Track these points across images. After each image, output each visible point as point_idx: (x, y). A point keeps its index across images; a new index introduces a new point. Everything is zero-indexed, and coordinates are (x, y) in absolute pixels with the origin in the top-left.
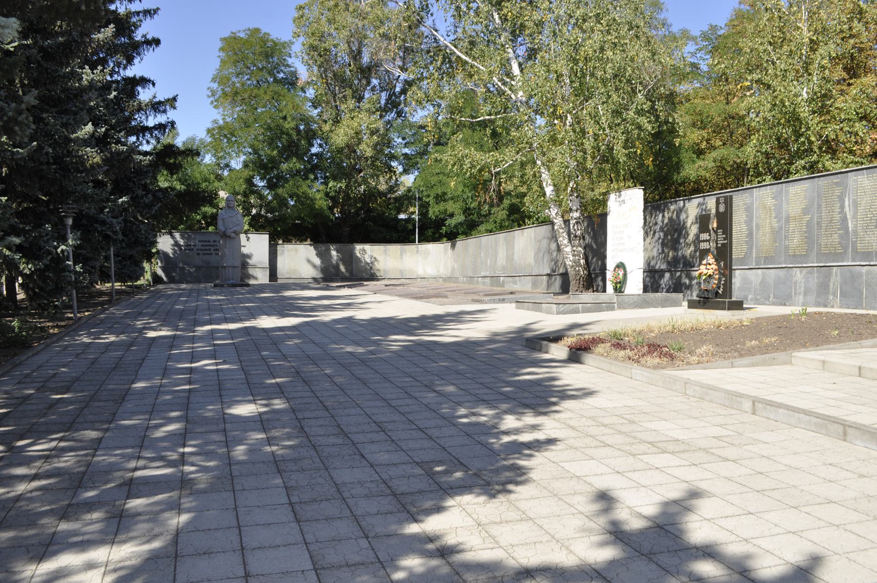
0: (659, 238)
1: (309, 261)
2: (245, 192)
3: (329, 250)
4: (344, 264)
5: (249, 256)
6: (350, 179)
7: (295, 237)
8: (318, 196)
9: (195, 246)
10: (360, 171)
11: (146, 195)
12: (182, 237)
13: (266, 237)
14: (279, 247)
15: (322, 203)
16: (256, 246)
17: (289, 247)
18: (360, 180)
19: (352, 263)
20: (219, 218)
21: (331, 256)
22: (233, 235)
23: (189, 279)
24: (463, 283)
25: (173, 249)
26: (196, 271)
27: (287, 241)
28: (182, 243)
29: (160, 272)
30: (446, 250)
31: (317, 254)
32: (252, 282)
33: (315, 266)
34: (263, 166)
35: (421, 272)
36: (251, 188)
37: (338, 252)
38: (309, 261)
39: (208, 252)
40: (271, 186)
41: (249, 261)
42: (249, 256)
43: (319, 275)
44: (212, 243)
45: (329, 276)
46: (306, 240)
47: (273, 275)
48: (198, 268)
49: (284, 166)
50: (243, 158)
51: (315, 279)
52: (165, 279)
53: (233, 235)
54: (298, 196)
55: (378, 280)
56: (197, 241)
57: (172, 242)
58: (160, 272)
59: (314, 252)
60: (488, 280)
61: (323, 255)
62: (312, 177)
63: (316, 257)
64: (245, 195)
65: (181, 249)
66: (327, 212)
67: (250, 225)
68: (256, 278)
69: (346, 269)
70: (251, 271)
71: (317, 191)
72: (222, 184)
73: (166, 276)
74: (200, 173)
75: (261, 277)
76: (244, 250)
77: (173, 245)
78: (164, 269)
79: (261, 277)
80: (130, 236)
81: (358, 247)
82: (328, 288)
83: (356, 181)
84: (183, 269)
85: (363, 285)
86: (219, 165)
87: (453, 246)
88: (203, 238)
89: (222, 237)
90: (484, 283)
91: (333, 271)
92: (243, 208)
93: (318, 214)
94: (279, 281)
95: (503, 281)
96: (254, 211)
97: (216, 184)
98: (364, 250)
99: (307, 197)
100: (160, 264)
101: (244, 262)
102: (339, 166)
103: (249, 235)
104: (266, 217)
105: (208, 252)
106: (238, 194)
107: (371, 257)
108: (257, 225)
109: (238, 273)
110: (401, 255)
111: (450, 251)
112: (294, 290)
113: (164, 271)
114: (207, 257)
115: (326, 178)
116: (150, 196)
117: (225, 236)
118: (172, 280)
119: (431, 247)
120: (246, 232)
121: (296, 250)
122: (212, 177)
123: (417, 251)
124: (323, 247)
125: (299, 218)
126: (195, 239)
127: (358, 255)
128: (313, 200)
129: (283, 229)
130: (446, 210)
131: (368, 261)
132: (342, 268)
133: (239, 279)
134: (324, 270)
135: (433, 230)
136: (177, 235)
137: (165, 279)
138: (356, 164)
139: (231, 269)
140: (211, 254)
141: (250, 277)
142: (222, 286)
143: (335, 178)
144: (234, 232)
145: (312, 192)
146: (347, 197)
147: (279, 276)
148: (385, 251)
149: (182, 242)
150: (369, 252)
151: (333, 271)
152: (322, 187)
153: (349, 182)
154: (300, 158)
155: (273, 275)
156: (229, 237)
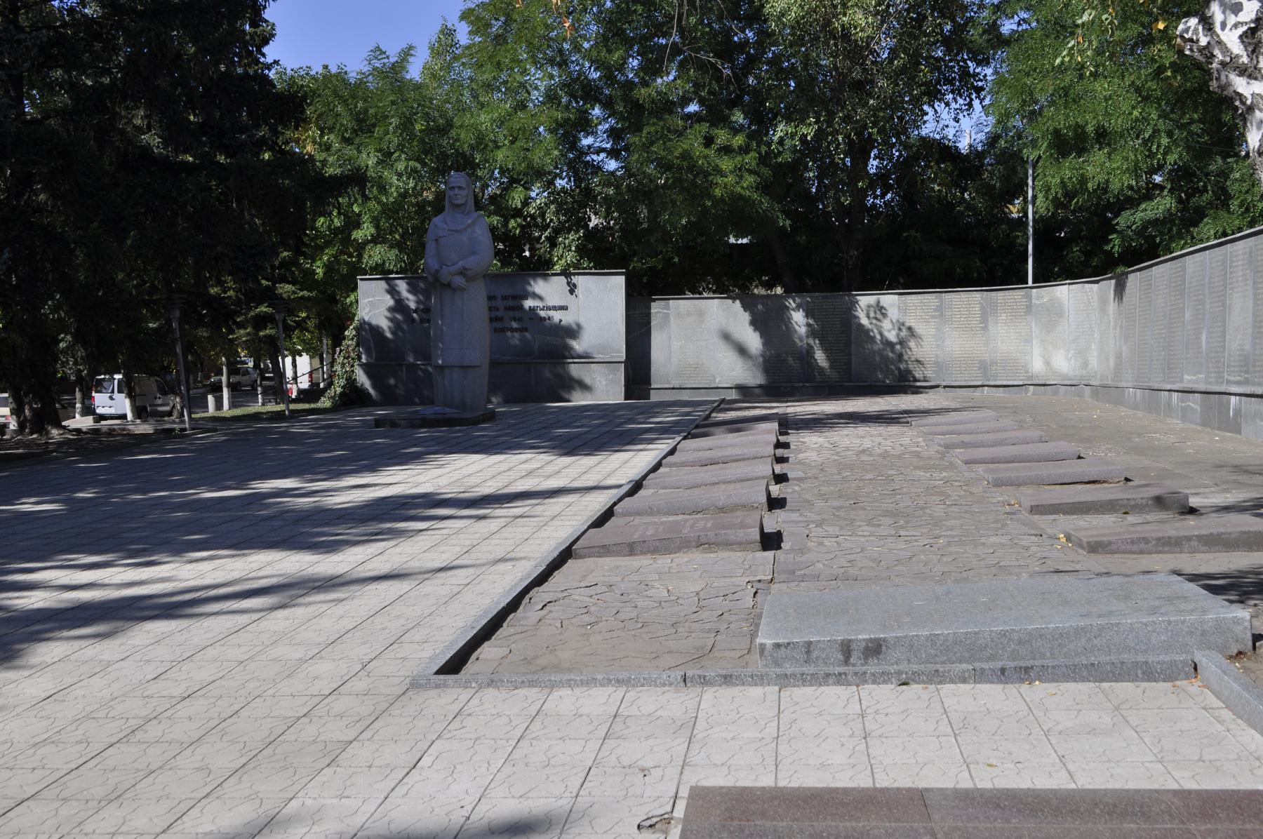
0: (295, 378)
1: (726, 337)
4: (826, 350)
5: (572, 332)
6: (831, 115)
12: (413, 289)
13: (617, 284)
14: (656, 308)
16: (590, 307)
21: (789, 329)
22: (459, 281)
24: (1135, 407)
28: (413, 306)
29: (362, 378)
30: (1103, 302)
32: (579, 400)
33: (742, 350)
35: (1037, 366)
38: (726, 337)
42: (572, 332)
51: (743, 390)
55: (917, 391)
57: (390, 302)
58: (362, 378)
59: (746, 317)
60: (1194, 402)
61: (768, 321)
67: (581, 250)
69: (829, 358)
73: (374, 386)
77: (391, 309)
78: (368, 369)
79: (604, 388)
81: (865, 301)
87: (1120, 290)
90: (1185, 414)
94: (655, 397)
95: (1238, 412)
98: (880, 308)
103: (575, 279)
107: (900, 326)
108: (599, 255)
110: (984, 320)
111: (1112, 306)
113: (369, 374)
118: (388, 397)
119: (1064, 293)
121: (701, 314)
123: (1029, 308)
127: (864, 321)
130: (1083, 180)
131: (892, 336)
132: (820, 357)
135: (1087, 245)
136: (402, 286)
148: (939, 309)
150: (893, 313)
153: (830, 122)
156: (449, 285)
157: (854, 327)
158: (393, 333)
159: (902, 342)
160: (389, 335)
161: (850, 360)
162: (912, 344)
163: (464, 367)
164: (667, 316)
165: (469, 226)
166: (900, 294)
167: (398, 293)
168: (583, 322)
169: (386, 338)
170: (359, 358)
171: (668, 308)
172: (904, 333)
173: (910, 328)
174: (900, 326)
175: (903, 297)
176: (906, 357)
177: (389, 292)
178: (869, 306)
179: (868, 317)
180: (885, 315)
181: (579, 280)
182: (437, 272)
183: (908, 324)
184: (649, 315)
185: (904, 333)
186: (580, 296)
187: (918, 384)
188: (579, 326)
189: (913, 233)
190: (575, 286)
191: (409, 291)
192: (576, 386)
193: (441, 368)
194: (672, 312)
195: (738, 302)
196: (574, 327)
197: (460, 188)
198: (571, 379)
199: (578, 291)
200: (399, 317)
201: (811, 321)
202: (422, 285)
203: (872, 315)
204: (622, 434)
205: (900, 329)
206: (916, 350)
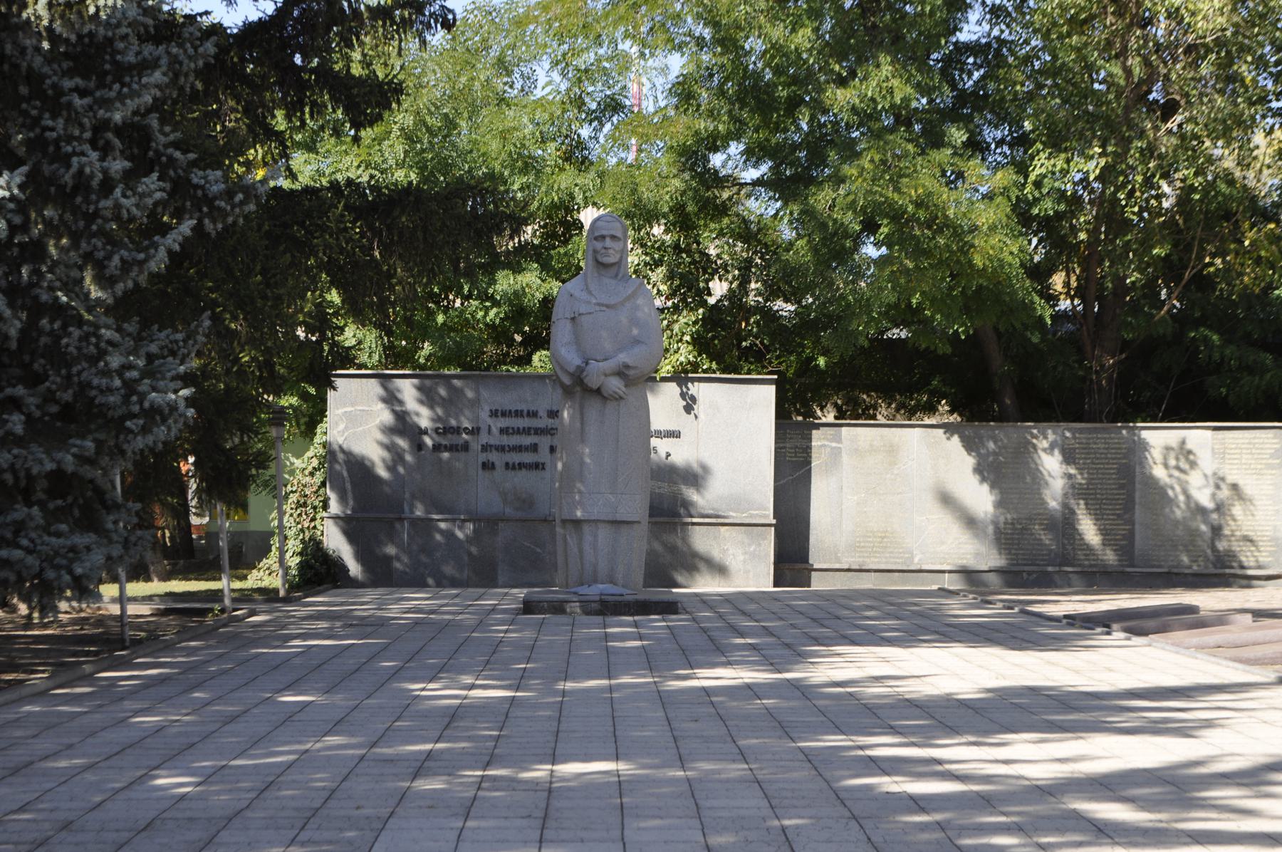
1: (946, 500)
2: (679, 209)
3: (1025, 451)
4: (1098, 517)
5: (695, 477)
6: (1125, 143)
7: (888, 397)
8: (986, 216)
9: (475, 432)
10: (1169, 109)
11: (130, 178)
12: (428, 397)
13: (762, 398)
14: (819, 439)
15: (1001, 247)
16: (722, 432)
17: (857, 436)
18: (1167, 144)
19: (1129, 505)
20: (558, 312)
22: (615, 384)
23: (448, 570)
25: (390, 448)
26: (476, 537)
27: (854, 412)
29: (335, 541)
31: (978, 470)
32: (706, 585)
33: (970, 522)
34: (757, 100)
36: (705, 200)
37: (1068, 458)
38: (946, 500)
39: (528, 458)
40: (786, 186)
41: (693, 495)
42: (695, 477)
43: (985, 557)
44: (543, 422)
45: (1033, 564)
46: (931, 409)
47: (792, 557)
48: (488, 523)
49: (841, 98)
50: (677, 64)
51: (968, 574)
52: (354, 568)
53: (615, 384)
54: (896, 216)
55: (1247, 581)
56: (484, 414)
57: (385, 416)
58: (335, 541)
59: (970, 461)
61: (1006, 473)
62: (958, 135)
63: (974, 480)
64: (682, 221)
65: (419, 446)
66: (1023, 286)
67: (699, 343)
68: (720, 570)
69: (1104, 532)
70: (702, 540)
71: (978, 198)
72: (588, 179)
73: (360, 556)
74: (504, 135)
75: (741, 566)
76: (678, 453)
77: (389, 430)
78: (350, 527)
79: (741, 566)
80: (54, 380)
81: (1158, 439)
82: (1021, 634)
83: (1149, 152)
84: (425, 526)
85: (1187, 618)
86: (579, 103)
88: (508, 400)
89: (568, 392)
91: (1046, 538)
92: (670, 277)
93: (985, 295)
94: (819, 583)
96: (719, 288)
97: (567, 179)
98: (1185, 453)
99: (937, 222)
100: (335, 507)
101: (669, 504)
102: (1077, 93)
103: (694, 389)
104: (770, 317)
105: (528, 458)
106: (650, 216)
107: (1218, 482)
108: (727, 346)
109: (634, 550)
112: (874, 638)
114: (522, 480)
115: (1023, 141)
116: (151, 182)
117: (579, 387)
118: (381, 574)
120: (682, 376)
121: (892, 450)
122: (551, 151)
124: (998, 437)
125: (903, 314)
126: (475, 403)
127: (1159, 472)
128: (960, 234)
129: (832, 370)
131: (1204, 498)
132: (1089, 530)
133: (639, 576)
134: (1009, 536)
136: (408, 390)
137: (354, 568)
138: (1149, 80)
139: (604, 533)
140: (538, 466)
141: (693, 562)
142: (558, 608)
143: (1057, 141)
144: (622, 373)
145: (953, 203)
146: (1111, 215)
147: (816, 560)
149: (424, 417)
150: (1207, 463)
151: (1046, 538)
152: (1004, 178)
153: (1121, 156)
154: (911, 56)
155: (792, 557)
157: (1138, 479)
158: (391, 469)
159: (1220, 508)
160: (382, 472)
161: (1132, 533)
162: (1237, 510)
163: (616, 523)
164: (836, 453)
165: (628, 298)
166: (1090, 431)
167: (401, 402)
168: (710, 462)
169: (378, 479)
170: (325, 506)
171: (840, 441)
172: (1225, 493)
173: (1235, 487)
174: (1218, 482)
175: (1221, 434)
176: (1226, 532)
177: (384, 400)
178: (1168, 449)
179: (1166, 466)
180: (1193, 464)
181: (700, 390)
182: (580, 370)
183: (1231, 479)
184: (807, 450)
185: (1225, 493)
186: (701, 416)
187: (1250, 572)
188: (705, 469)
189: (1205, 331)
190: (693, 399)
191: (421, 402)
192: (702, 565)
193: (577, 523)
194: (845, 445)
195: (956, 439)
196: (700, 471)
197: (613, 237)
198: (695, 555)
199: (699, 408)
200: (402, 443)
201: (1073, 471)
202: (442, 392)
203: (1172, 462)
204: (882, 638)
205: (1218, 487)
206: (1242, 521)
